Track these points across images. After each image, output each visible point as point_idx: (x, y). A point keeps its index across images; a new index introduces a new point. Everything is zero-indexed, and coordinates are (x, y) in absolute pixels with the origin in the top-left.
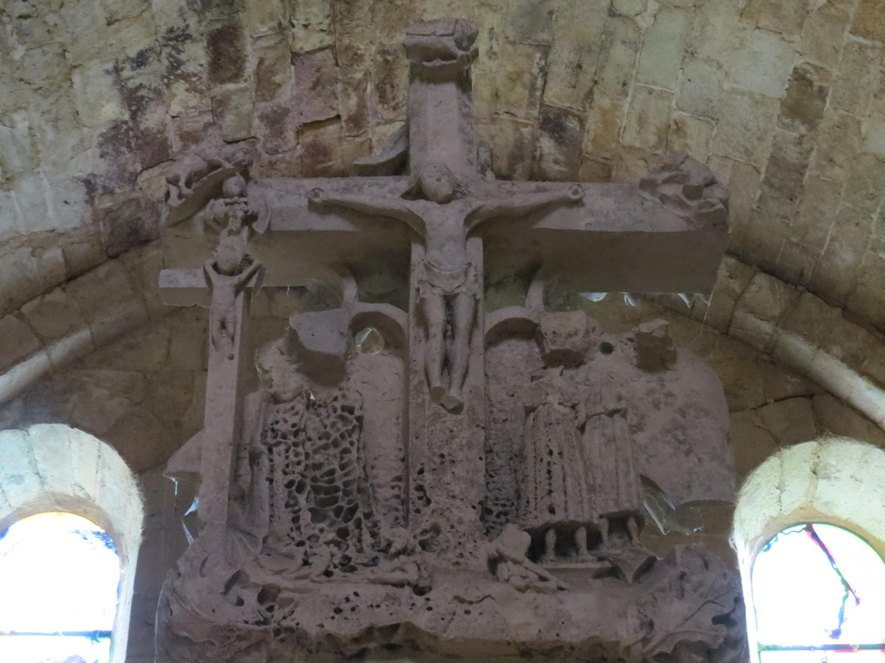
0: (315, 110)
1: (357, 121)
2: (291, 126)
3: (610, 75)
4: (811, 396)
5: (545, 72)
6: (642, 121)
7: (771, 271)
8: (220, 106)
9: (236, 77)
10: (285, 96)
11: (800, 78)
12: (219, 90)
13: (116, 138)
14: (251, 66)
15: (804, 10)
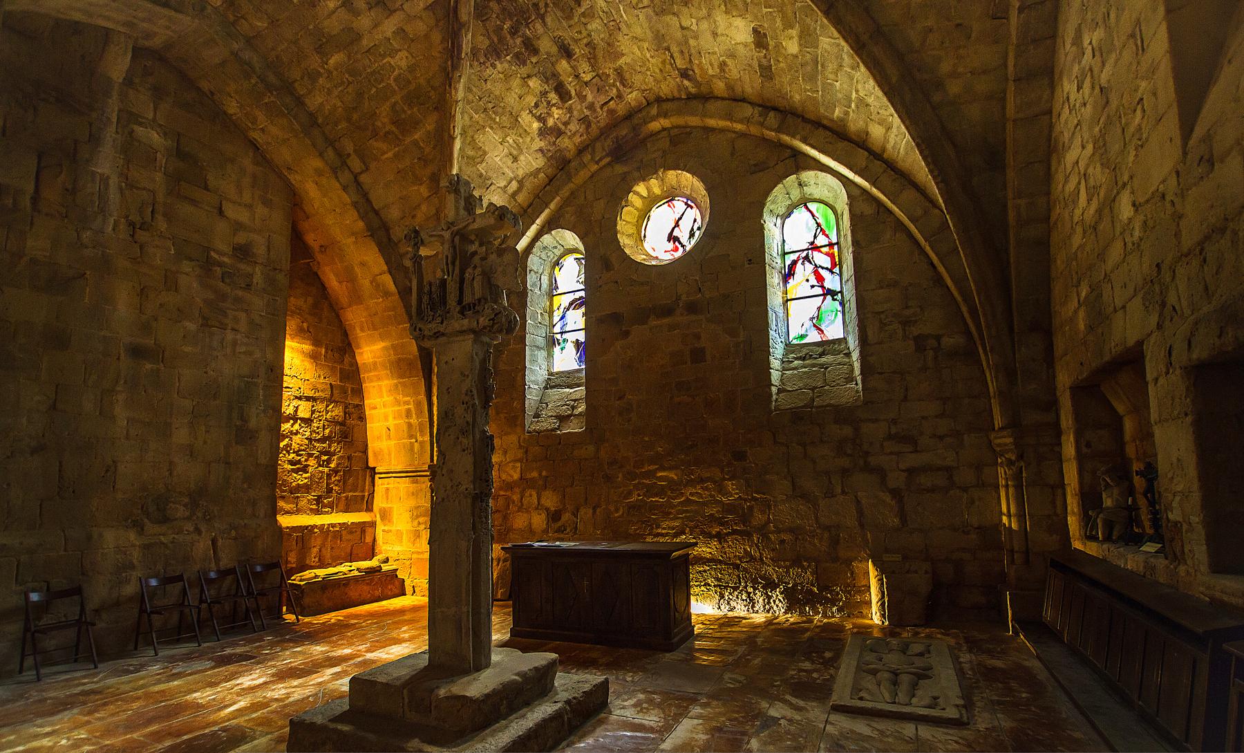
0: (603, 99)
1: (620, 96)
2: (597, 106)
3: (693, 51)
4: (794, 156)
5: (672, 56)
6: (711, 65)
7: (775, 109)
8: (570, 110)
9: (570, 98)
10: (590, 98)
11: (755, 31)
12: (566, 105)
13: (542, 133)
14: (573, 93)
15: (746, 4)
